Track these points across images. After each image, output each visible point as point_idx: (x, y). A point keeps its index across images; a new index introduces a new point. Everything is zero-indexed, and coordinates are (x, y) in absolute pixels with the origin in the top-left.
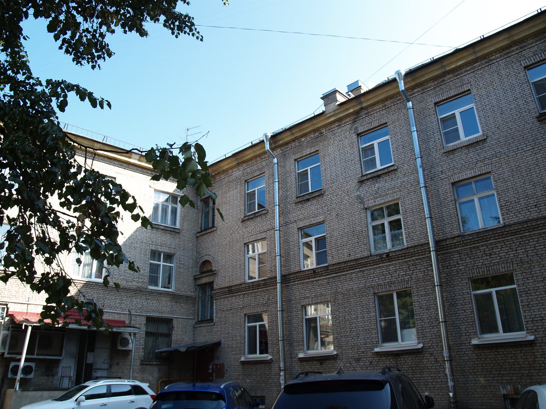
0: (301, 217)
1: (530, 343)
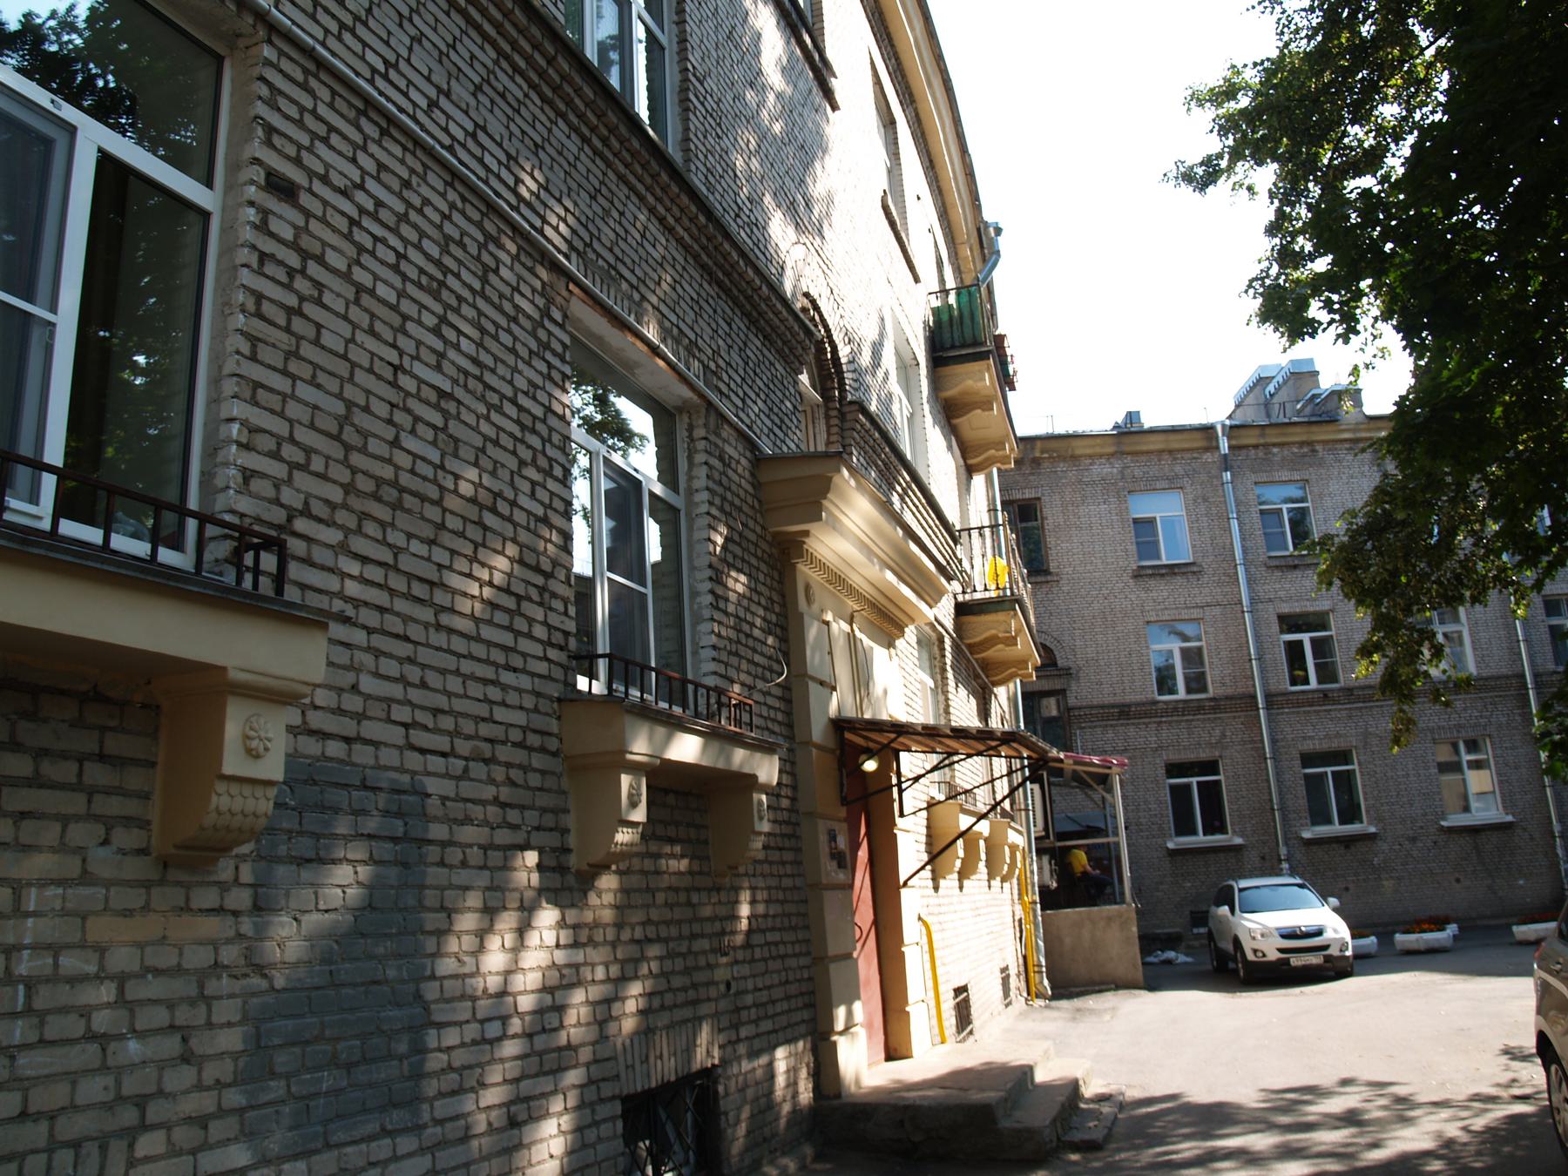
0: (1282, 594)
1: (1237, 849)
